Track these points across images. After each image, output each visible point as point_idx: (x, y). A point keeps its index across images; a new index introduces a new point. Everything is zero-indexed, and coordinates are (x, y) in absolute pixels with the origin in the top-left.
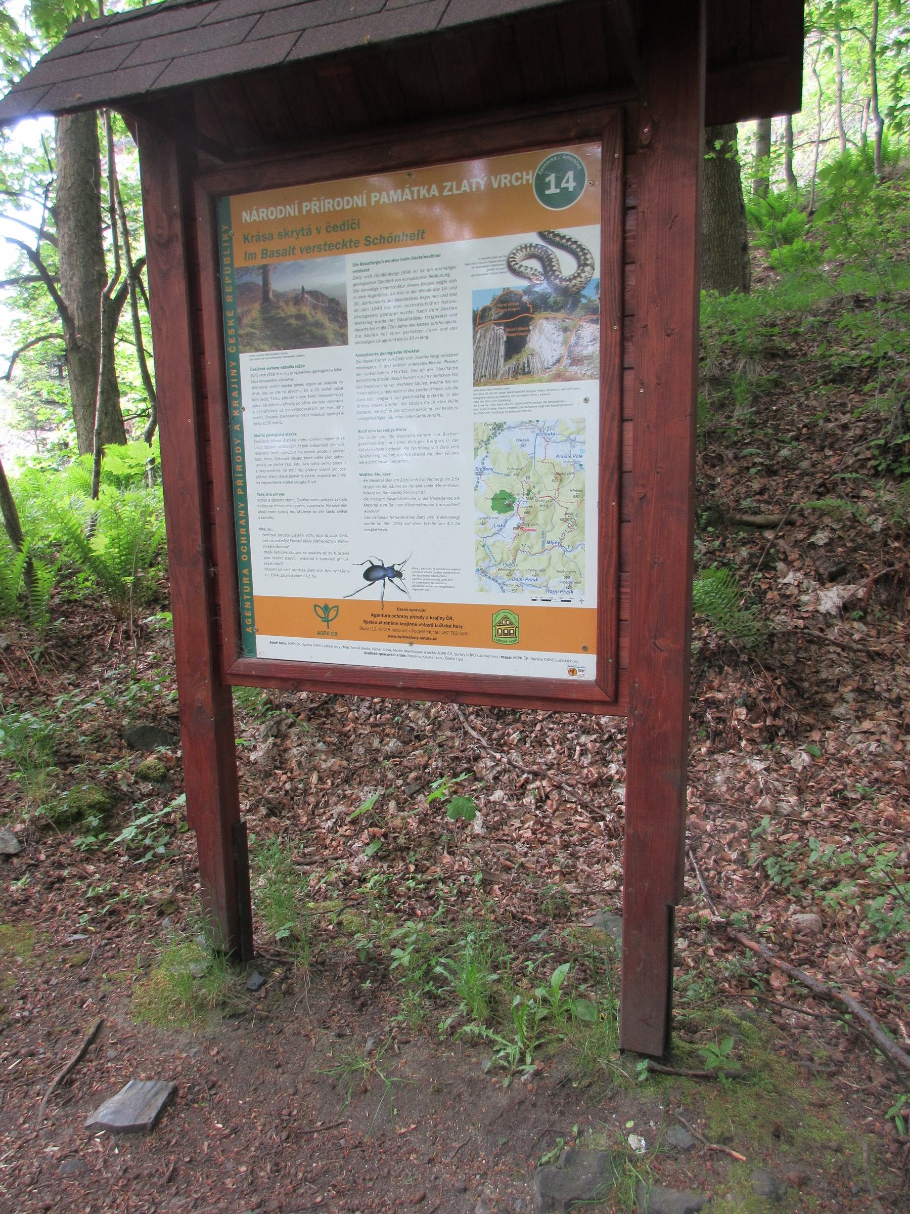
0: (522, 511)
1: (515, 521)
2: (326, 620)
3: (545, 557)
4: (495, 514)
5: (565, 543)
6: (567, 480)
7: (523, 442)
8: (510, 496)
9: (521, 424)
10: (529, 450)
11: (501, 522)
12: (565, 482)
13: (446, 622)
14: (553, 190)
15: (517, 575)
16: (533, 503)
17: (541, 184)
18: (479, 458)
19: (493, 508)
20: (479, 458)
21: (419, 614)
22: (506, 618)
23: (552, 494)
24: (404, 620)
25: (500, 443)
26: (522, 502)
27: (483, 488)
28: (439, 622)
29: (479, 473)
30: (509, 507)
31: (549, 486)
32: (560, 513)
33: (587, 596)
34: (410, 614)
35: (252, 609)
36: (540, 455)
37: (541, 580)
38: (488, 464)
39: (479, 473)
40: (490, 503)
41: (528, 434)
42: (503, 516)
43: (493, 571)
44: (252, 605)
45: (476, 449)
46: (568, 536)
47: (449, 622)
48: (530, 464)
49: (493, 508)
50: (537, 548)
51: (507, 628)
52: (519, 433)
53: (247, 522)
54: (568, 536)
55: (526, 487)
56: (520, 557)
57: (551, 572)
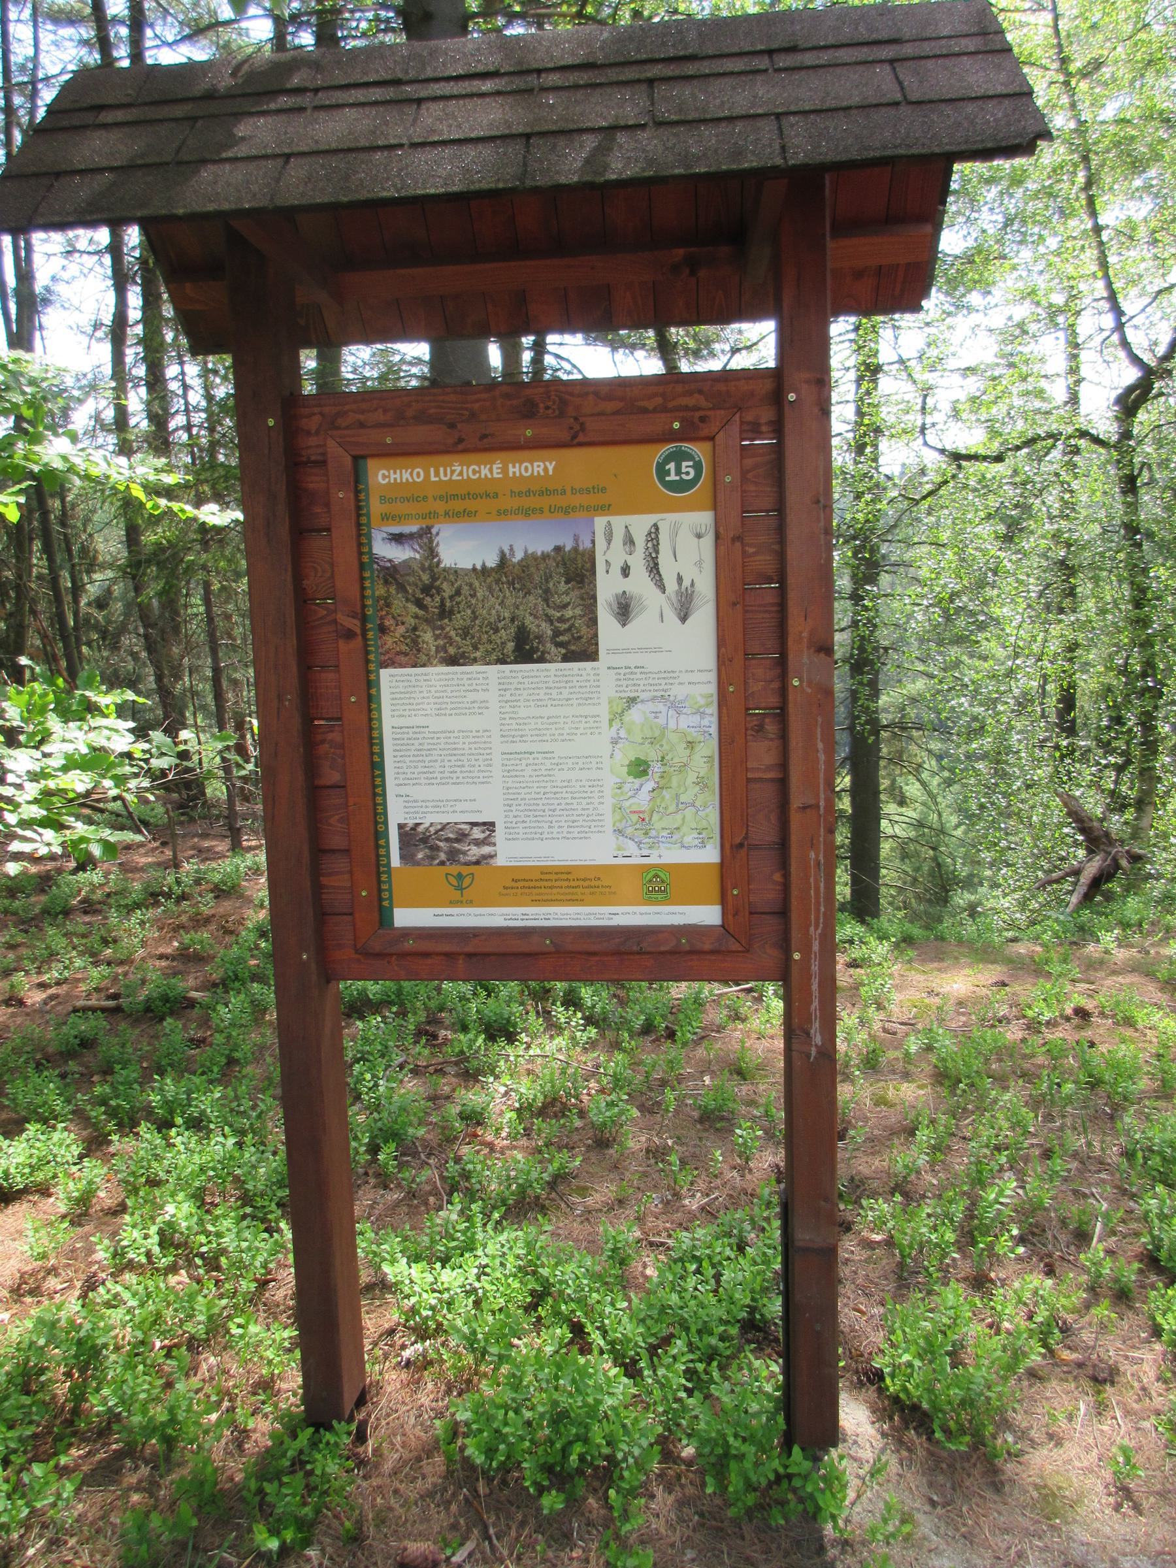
0: (657, 776)
1: (650, 785)
2: (460, 888)
3: (679, 817)
4: (631, 779)
5: (698, 804)
6: (698, 748)
7: (656, 714)
8: (645, 762)
9: (654, 699)
10: (661, 721)
11: (636, 786)
12: (697, 749)
13: (593, 883)
14: (673, 477)
15: (653, 833)
16: (667, 769)
17: (662, 472)
18: (614, 729)
19: (629, 774)
20: (614, 729)
21: (565, 876)
22: (656, 876)
23: (685, 760)
24: (549, 884)
25: (635, 715)
26: (656, 768)
27: (618, 755)
28: (586, 884)
29: (615, 742)
30: (644, 773)
31: (681, 752)
32: (692, 777)
33: (710, 855)
34: (554, 877)
35: (390, 882)
36: (672, 725)
37: (675, 837)
38: (623, 734)
39: (615, 742)
40: (625, 769)
41: (661, 707)
42: (638, 781)
43: (629, 830)
44: (390, 877)
45: (611, 721)
46: (701, 797)
47: (597, 883)
48: (663, 734)
49: (629, 774)
50: (672, 809)
51: (659, 884)
52: (651, 706)
53: (385, 809)
54: (701, 797)
55: (660, 755)
56: (655, 817)
57: (684, 829)
